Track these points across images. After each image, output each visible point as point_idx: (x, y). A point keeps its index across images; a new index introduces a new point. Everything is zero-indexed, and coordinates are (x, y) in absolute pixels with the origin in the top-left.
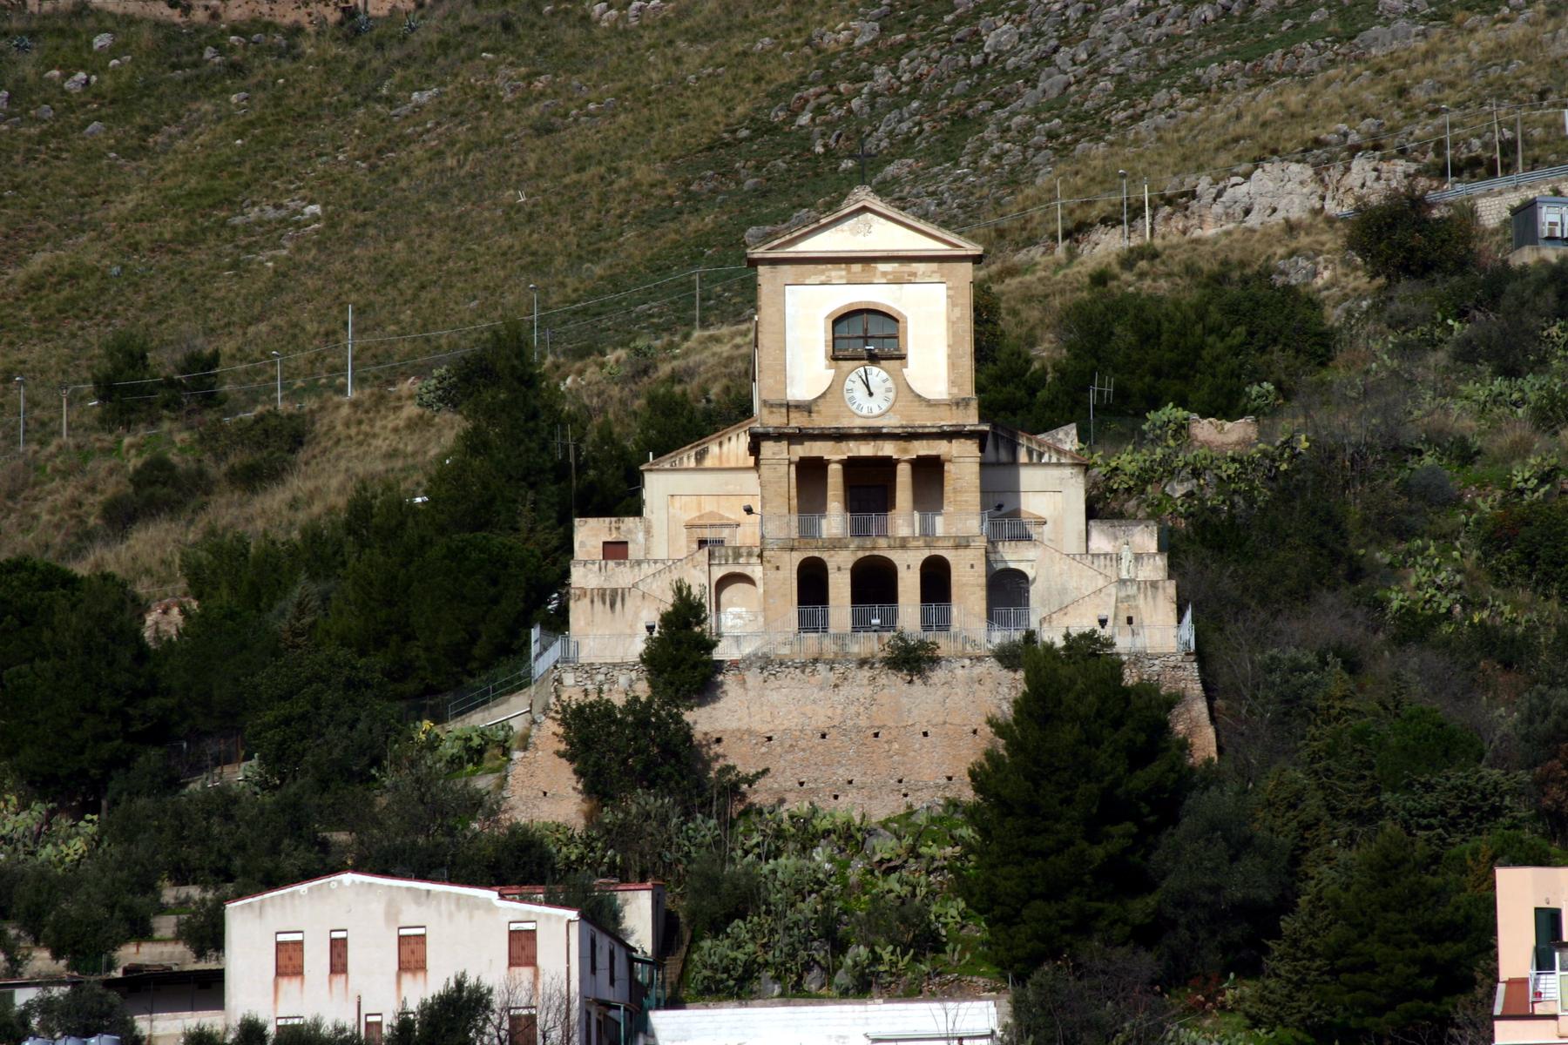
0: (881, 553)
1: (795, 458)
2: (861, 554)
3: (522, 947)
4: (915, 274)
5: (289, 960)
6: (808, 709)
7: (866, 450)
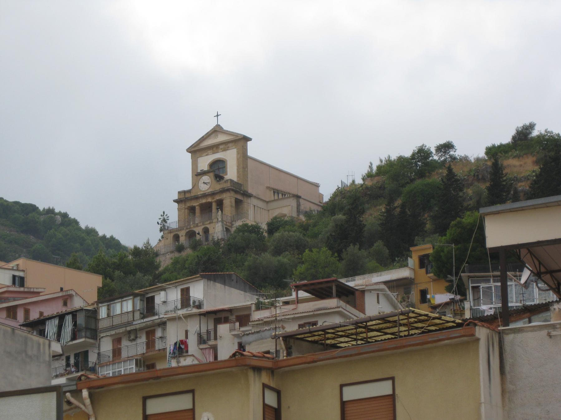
1: (186, 207)
2: (187, 231)
7: (204, 201)
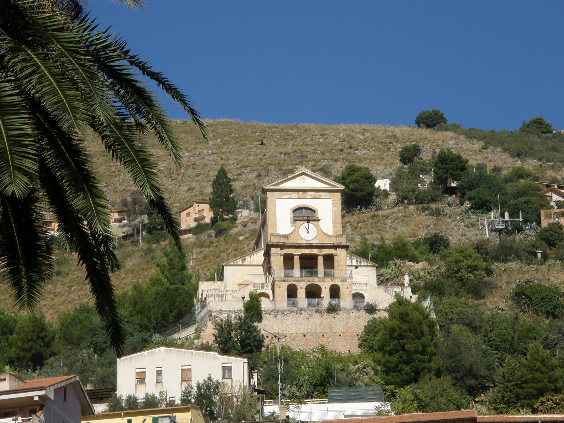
0: (316, 283)
2: (309, 283)
3: (226, 370)
4: (321, 196)
5: (141, 379)
6: (299, 327)
7: (307, 251)
